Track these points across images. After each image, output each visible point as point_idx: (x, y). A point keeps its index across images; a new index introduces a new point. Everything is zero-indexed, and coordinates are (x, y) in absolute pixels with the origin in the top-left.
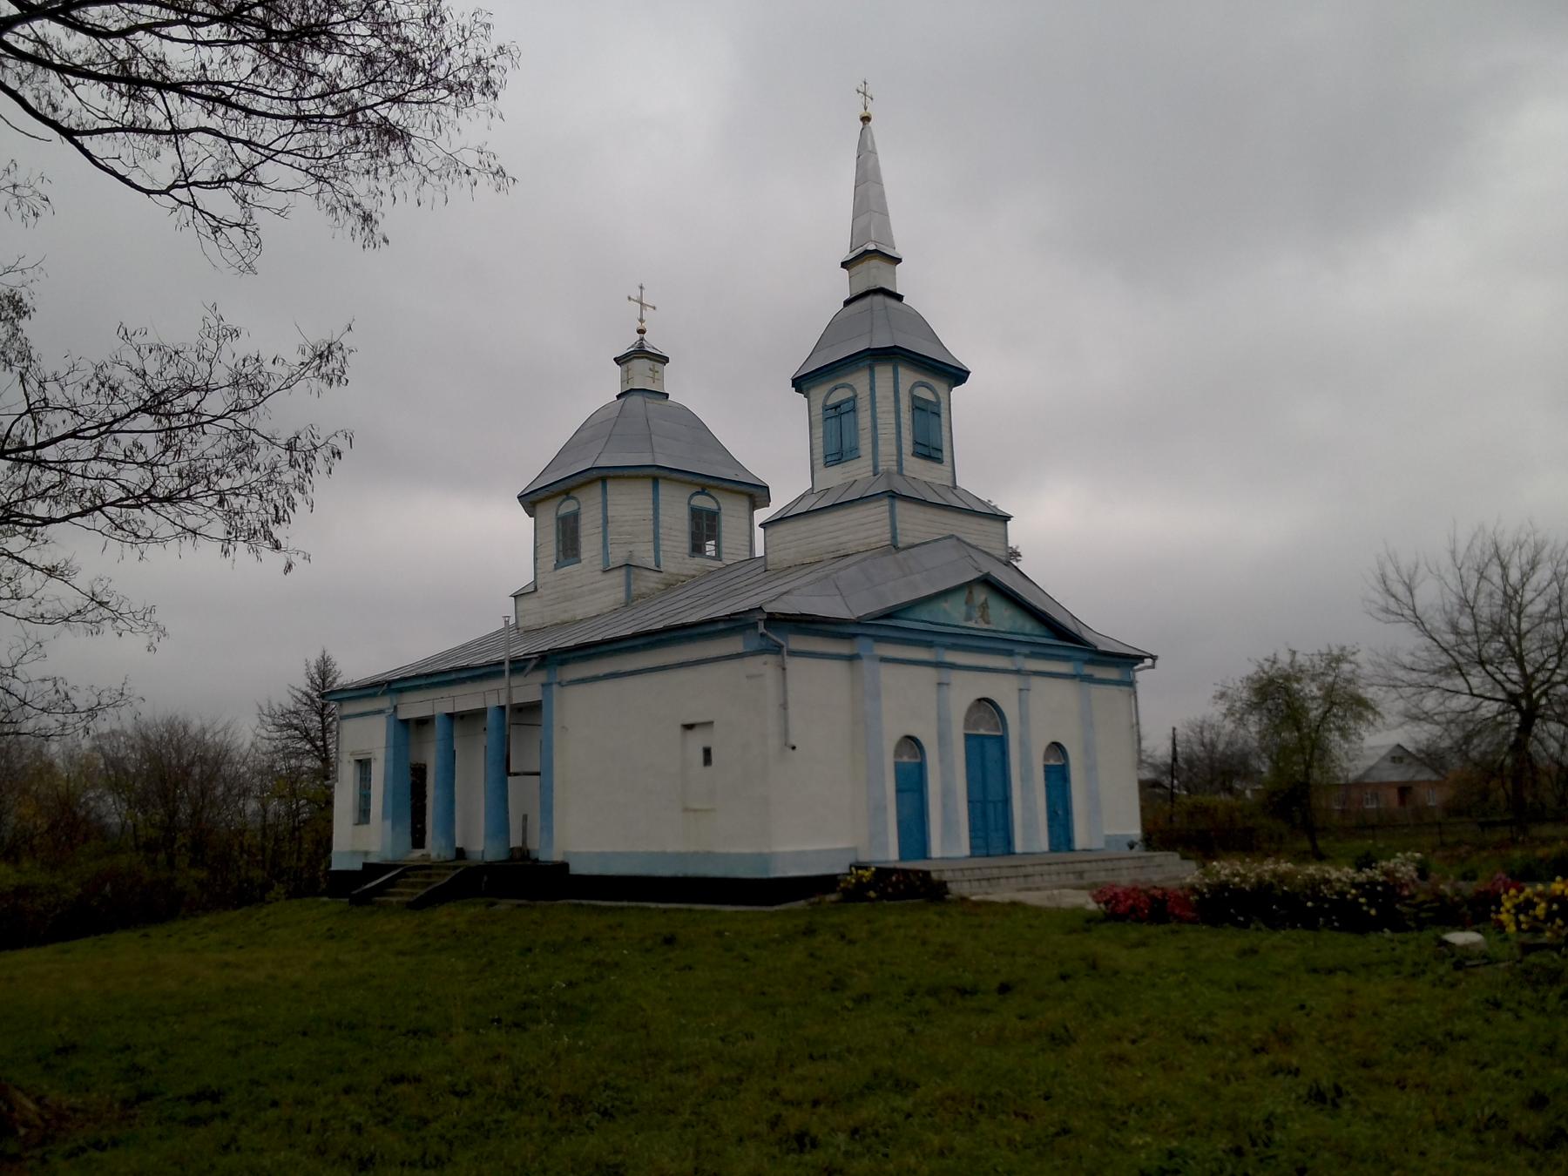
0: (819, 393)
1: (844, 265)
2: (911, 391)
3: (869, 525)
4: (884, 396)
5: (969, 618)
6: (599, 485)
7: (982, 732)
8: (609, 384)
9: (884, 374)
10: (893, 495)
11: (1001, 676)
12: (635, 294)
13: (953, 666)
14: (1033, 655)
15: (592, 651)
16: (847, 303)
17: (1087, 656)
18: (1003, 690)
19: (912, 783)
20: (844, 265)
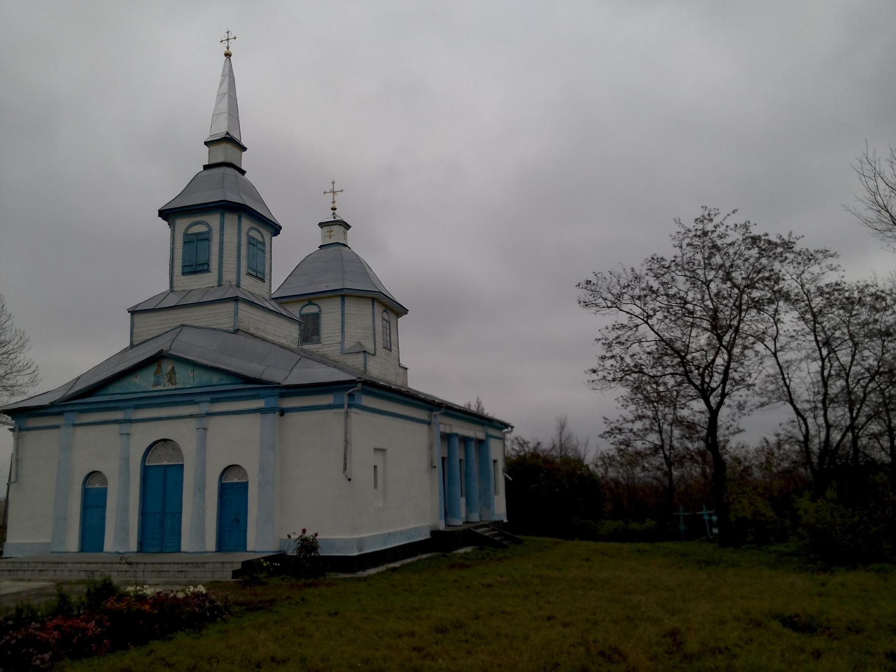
0: (182, 224)
1: (206, 143)
2: (248, 234)
3: (222, 316)
4: (230, 234)
5: (157, 383)
6: (339, 299)
7: (165, 463)
8: (317, 238)
9: (231, 220)
11: (399, 420)
12: (328, 188)
13: (131, 421)
14: (137, 407)
15: (415, 401)
16: (206, 167)
17: (277, 391)
18: (183, 433)
19: (93, 500)
20: (206, 143)
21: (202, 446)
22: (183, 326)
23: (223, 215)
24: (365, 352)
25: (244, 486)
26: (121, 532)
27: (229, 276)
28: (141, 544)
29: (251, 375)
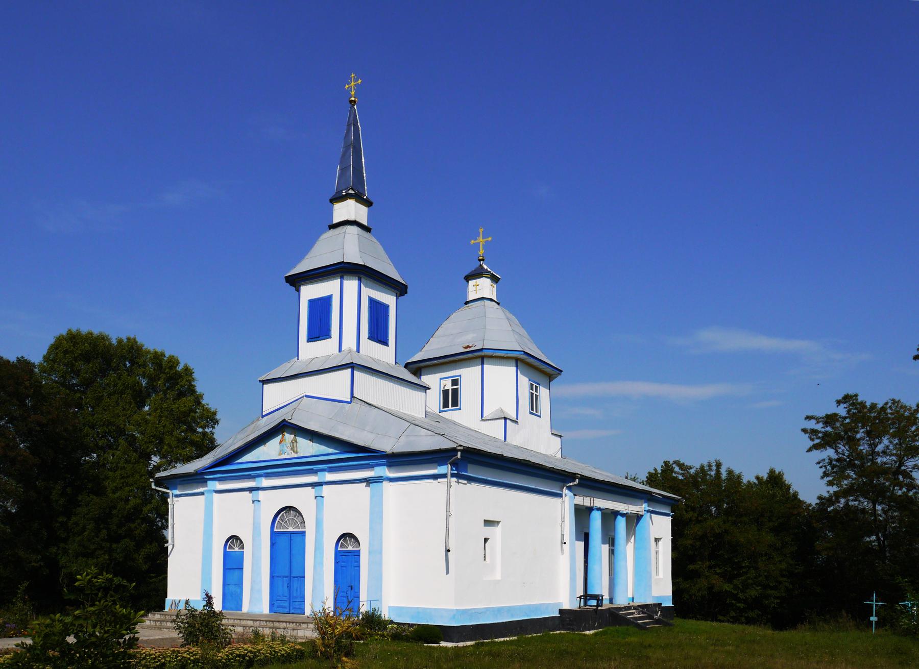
3: (336, 385)
6: (480, 361)
7: (291, 529)
9: (351, 285)
10: (352, 366)
19: (233, 565)
21: (319, 508)
22: (307, 396)
23: (342, 278)
24: (505, 419)
25: (357, 554)
26: (256, 599)
27: (349, 342)
28: (272, 605)
29: (361, 443)
